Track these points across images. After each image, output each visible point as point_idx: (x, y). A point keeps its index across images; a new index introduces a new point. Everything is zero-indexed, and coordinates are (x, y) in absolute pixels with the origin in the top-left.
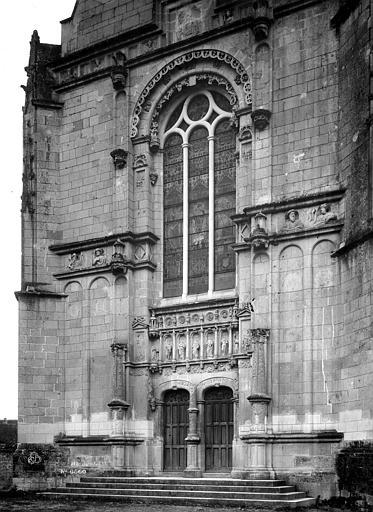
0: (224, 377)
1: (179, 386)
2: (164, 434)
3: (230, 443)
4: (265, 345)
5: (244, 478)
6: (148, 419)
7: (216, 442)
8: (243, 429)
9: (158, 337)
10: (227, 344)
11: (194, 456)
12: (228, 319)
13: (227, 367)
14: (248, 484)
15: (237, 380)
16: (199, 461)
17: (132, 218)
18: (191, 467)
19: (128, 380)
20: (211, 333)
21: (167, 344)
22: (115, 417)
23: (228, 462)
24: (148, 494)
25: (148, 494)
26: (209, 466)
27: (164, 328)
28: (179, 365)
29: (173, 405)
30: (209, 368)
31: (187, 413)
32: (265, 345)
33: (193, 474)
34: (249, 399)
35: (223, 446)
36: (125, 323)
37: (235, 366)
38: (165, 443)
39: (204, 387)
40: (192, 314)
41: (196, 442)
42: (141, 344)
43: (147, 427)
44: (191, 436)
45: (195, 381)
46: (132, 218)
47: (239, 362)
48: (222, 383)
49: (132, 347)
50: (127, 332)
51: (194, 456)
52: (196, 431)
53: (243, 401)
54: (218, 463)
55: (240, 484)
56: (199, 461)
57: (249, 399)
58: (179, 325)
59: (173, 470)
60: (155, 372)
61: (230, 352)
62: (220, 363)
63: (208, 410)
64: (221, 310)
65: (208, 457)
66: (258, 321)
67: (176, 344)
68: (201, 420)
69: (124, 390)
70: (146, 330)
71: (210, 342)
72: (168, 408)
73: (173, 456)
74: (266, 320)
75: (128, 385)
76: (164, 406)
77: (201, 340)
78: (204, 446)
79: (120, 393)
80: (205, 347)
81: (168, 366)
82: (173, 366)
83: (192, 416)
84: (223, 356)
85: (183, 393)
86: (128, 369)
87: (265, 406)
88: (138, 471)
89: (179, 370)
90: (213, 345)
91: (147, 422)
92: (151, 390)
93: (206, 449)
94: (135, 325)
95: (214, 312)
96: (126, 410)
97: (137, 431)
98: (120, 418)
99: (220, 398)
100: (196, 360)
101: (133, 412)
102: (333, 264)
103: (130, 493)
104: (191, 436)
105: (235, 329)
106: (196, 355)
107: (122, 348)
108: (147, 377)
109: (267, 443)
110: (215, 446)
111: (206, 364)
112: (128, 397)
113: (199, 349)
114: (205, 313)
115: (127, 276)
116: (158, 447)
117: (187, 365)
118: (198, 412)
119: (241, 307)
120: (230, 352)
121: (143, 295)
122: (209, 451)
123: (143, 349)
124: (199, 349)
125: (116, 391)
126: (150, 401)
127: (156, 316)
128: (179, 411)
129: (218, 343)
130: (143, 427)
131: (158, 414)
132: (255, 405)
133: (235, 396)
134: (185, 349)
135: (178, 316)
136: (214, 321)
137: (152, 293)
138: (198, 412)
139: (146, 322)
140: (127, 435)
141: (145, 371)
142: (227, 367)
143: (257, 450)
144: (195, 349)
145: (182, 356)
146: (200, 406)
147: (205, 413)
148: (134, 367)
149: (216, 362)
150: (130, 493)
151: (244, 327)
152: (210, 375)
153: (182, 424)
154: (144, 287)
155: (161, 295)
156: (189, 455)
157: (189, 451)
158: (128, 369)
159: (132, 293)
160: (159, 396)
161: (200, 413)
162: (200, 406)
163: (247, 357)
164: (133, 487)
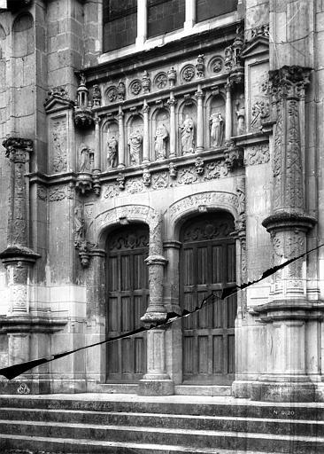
0: (215, 190)
1: (132, 217)
2: (106, 311)
3: (231, 325)
4: (302, 103)
5: (258, 398)
6: (75, 282)
7: (203, 323)
8: (256, 295)
9: (92, 127)
10: (222, 124)
11: (159, 352)
12: (225, 71)
13: (222, 169)
14: (266, 412)
15: (242, 191)
16: (170, 362)
17: (30, 353)
18: (153, 374)
19: (35, 208)
20: (190, 106)
21: (108, 137)
22: (12, 278)
23: (226, 364)
24: (49, 432)
25: (49, 432)
26: (188, 374)
27: (104, 104)
28: (130, 175)
29: (123, 256)
30: (188, 176)
31: (146, 266)
32: (302, 103)
33: (156, 388)
34: (265, 224)
35: (216, 331)
36: (29, 103)
37: (237, 166)
38: (109, 329)
39: (178, 214)
40: (154, 73)
41: (161, 324)
42: (60, 141)
43: (72, 298)
44: (153, 313)
45: (156, 203)
46: (30, 353)
47: (246, 153)
48: (212, 202)
49: (45, 147)
50: (33, 119)
51: (159, 352)
52: (162, 303)
53: (256, 233)
54: (206, 364)
55: (246, 411)
56: (170, 362)
57: (265, 224)
58: (130, 97)
59: (123, 380)
60: (87, 192)
61: (228, 136)
62: (209, 161)
63: (187, 261)
64: (208, 58)
65: (187, 354)
66: (282, 56)
67: (126, 135)
68: (172, 280)
69: (29, 225)
70: (68, 113)
71: (188, 122)
72: (114, 261)
73: (121, 352)
74: (304, 52)
75: (35, 217)
76: (106, 256)
77: (174, 121)
78: (178, 332)
79: (19, 232)
80: (179, 134)
81: (110, 179)
82: (120, 178)
83: (154, 272)
84: (215, 147)
85: (139, 228)
86: (35, 188)
87: (301, 237)
88: (56, 382)
89: (131, 185)
90: (194, 129)
91: (72, 288)
92: (79, 226)
93: (185, 337)
94: (50, 105)
95: (195, 62)
96: (32, 264)
97: (54, 307)
98: (20, 280)
99: (210, 231)
100: (161, 160)
101: (47, 268)
102: (258, 330)
103: (16, 430)
104: (153, 313)
105: (238, 89)
106: (163, 152)
107: (23, 148)
108: (71, 203)
109: (307, 321)
110: (201, 332)
111: (182, 167)
112: (35, 240)
113: (167, 140)
114: (179, 67)
115: (33, 12)
116: (95, 333)
117: (146, 173)
118: (165, 264)
119: (249, 37)
120: (228, 136)
121: (62, 47)
122: (188, 341)
123: (66, 151)
124: (167, 140)
125: (12, 229)
126: (77, 248)
127: (89, 85)
128: (133, 265)
129: (200, 125)
130: (67, 298)
131: (93, 274)
132: (280, 236)
133: (240, 226)
134: (141, 142)
135: (127, 81)
136: (197, 79)
137: (80, 43)
138: (165, 264)
139: (70, 96)
140: (35, 313)
141: (66, 191)
142: (222, 169)
143: (284, 333)
144: (160, 141)
145: (136, 157)
146: (171, 252)
147: (181, 266)
148: (47, 183)
149: (199, 162)
150: (16, 430)
151: (256, 79)
152: (189, 190)
153: (139, 291)
154: (65, 30)
155: (98, 46)
156: (149, 352)
157: (149, 344)
158: (35, 188)
159: (43, 42)
160: (95, 238)
161: (172, 266)
162: (171, 252)
163: (262, 140)
164: (26, 416)
